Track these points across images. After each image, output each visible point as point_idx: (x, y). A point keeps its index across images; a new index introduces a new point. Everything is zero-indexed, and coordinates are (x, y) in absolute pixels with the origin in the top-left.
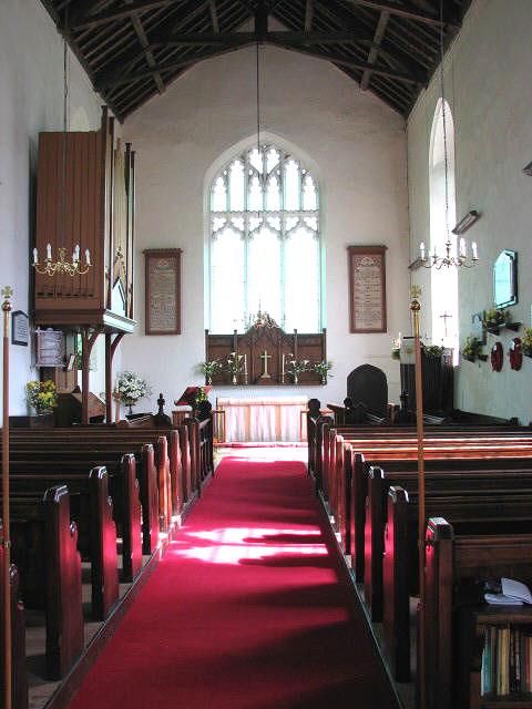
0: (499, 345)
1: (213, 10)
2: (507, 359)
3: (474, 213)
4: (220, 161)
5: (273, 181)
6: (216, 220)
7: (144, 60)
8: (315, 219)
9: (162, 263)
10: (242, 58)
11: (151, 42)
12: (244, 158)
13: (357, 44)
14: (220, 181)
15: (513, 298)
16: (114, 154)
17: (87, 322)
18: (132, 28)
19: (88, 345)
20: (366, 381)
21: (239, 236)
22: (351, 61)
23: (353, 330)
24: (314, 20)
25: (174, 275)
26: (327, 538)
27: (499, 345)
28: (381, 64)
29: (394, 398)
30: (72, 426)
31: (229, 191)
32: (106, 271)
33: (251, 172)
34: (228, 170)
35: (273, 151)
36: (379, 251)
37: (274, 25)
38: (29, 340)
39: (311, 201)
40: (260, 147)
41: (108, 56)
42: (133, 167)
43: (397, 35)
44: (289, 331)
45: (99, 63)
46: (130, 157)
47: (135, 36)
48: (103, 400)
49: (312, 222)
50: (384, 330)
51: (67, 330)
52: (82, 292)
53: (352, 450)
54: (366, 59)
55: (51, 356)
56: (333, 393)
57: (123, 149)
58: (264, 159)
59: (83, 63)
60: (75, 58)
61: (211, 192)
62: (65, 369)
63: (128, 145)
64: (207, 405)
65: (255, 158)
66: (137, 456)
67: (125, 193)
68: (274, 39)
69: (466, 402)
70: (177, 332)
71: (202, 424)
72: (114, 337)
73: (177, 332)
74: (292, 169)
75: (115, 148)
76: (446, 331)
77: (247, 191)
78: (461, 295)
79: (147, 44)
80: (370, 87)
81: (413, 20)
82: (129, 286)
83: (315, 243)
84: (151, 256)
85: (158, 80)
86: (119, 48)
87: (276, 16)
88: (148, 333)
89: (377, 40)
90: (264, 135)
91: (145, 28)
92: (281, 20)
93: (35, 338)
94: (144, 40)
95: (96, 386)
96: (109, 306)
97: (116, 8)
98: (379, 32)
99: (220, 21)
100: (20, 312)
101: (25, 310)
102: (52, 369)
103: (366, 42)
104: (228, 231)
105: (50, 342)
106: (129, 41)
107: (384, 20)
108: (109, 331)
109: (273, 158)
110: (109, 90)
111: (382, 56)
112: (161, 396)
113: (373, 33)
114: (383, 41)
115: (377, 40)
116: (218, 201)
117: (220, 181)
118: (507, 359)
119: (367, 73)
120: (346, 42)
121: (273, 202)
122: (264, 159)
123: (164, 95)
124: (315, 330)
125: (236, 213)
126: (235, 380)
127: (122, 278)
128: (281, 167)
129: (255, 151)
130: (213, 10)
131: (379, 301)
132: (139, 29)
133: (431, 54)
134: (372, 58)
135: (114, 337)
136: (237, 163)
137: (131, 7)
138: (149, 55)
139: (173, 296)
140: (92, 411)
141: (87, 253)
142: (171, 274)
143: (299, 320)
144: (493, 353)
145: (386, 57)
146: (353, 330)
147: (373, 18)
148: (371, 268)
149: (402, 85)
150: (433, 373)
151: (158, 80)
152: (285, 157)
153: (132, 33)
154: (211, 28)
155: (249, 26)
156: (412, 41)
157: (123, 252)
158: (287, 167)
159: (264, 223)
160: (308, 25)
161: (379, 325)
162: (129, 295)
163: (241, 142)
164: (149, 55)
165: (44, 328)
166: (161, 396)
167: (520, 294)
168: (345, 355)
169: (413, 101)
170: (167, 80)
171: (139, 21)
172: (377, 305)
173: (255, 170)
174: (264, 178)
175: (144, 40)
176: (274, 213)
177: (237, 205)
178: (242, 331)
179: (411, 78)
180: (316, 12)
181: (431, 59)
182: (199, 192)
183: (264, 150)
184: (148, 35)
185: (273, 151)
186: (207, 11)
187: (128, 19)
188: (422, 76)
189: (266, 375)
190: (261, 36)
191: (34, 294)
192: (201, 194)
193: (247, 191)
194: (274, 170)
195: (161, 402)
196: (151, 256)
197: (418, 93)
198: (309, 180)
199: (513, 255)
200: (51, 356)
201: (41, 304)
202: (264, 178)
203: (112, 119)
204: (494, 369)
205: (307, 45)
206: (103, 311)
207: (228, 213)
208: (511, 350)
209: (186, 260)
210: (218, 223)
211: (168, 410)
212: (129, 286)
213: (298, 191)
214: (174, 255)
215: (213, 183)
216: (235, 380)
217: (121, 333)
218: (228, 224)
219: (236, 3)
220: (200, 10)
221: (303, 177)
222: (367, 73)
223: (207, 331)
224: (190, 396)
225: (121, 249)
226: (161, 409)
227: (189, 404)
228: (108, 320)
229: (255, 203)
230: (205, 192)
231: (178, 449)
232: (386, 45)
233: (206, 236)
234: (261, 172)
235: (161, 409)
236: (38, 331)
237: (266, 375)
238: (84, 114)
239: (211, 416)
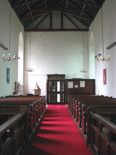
7: (30, 15)
41: (26, 10)
54: (80, 15)
67: (102, 42)
78: (18, 53)
84: (106, 84)
94: (30, 9)
97: (22, 2)
120: (73, 11)
132: (29, 7)
134: (81, 15)
137: (26, 2)
145: (84, 14)
153: (27, 8)
175: (30, 9)
187: (26, 5)
227: (93, 146)
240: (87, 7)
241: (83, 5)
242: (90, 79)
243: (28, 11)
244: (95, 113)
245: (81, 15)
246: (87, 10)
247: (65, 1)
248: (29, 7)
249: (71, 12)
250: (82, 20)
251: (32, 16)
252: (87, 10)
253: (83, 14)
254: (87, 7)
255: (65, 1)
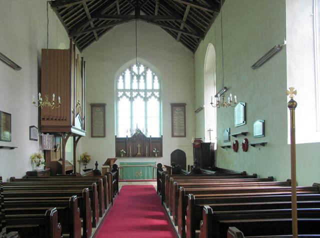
0: (237, 141)
1: (118, 6)
2: (241, 147)
3: (225, 88)
4: (121, 69)
5: (142, 77)
6: (119, 93)
7: (90, 26)
8: (158, 93)
9: (98, 109)
10: (131, 24)
11: (92, 17)
12: (130, 68)
13: (176, 22)
14: (121, 77)
15: (244, 122)
16: (76, 61)
17: (64, 131)
18: (84, 10)
19: (65, 141)
20: (178, 156)
21: (128, 99)
22: (171, 28)
23: (173, 136)
24: (159, 12)
25: (102, 114)
26: (166, 218)
27: (237, 142)
28: (185, 30)
29: (190, 161)
30: (57, 176)
31: (124, 82)
32: (72, 110)
33: (133, 74)
34: (124, 73)
35: (142, 66)
36: (183, 106)
37: (142, 13)
38: (38, 138)
39: (157, 86)
40: (137, 64)
41: (74, 22)
42: (84, 67)
43: (192, 17)
44: (148, 136)
45: (71, 25)
46: (83, 64)
47: (85, 14)
48: (72, 163)
49: (157, 94)
50: (185, 136)
51: (56, 135)
52: (62, 118)
53: (178, 184)
55: (49, 146)
56: (166, 160)
57: (80, 59)
58: (138, 69)
59: (63, 23)
60: (60, 21)
61: (117, 82)
62: (55, 151)
63: (82, 58)
64: (115, 166)
65: (135, 68)
66: (97, 183)
67: (81, 78)
68: (143, 18)
69: (220, 164)
70: (104, 136)
71: (114, 174)
72: (76, 138)
73: (104, 136)
74: (149, 73)
75: (76, 58)
76: (211, 134)
77: (132, 82)
78: (218, 122)
79: (90, 18)
80: (181, 41)
81: (196, 8)
82: (83, 117)
83: (158, 102)
84: (93, 106)
85: (96, 35)
86: (79, 19)
87: (143, 10)
88: (92, 136)
89: (184, 20)
90: (138, 59)
91: (90, 11)
92: (144, 12)
93: (41, 137)
94: (90, 17)
95: (69, 157)
96: (74, 125)
98: (185, 16)
99: (121, 12)
100: (34, 126)
101: (37, 125)
102: (49, 151)
103: (179, 21)
104: (124, 97)
105: (47, 138)
106: (82, 17)
107: (187, 11)
108: (75, 135)
109: (142, 68)
110: (76, 37)
111: (186, 27)
112: (97, 162)
113: (182, 17)
114: (187, 20)
115: (184, 20)
116: (120, 86)
117: (121, 77)
118: (241, 147)
119: (180, 33)
120: (170, 20)
121: (142, 87)
122: (138, 69)
123: (98, 41)
124: (158, 136)
125: (128, 90)
126: (122, 155)
127: (80, 113)
128: (145, 72)
129: (135, 66)
130: (118, 6)
131: (183, 125)
132: (87, 11)
133: (206, 25)
134: (181, 28)
135: (76, 138)
136: (128, 70)
138: (92, 23)
139: (102, 123)
140: (67, 167)
141: (59, 98)
142: (101, 114)
143: (153, 132)
144: (234, 145)
145: (187, 27)
146: (173, 136)
147: (182, 10)
148: (180, 112)
149: (202, 11)
150: (205, 153)
151: (96, 35)
152: (146, 68)
154: (117, 14)
155: (133, 13)
156: (198, 20)
157: (80, 103)
158: (147, 72)
159: (139, 94)
160: (156, 14)
161: (183, 134)
162: (83, 121)
163: (130, 61)
164: (92, 23)
165: (45, 133)
166: (97, 162)
167: (248, 121)
168: (169, 148)
169: (197, 46)
170: (100, 34)
171: (87, 8)
172: (182, 126)
173: (134, 73)
174: (138, 77)
175: (90, 17)
176: (142, 91)
177: (128, 87)
178: (129, 136)
179: (196, 35)
180: (159, 8)
181: (206, 28)
182: (113, 82)
183: (138, 66)
184: (91, 14)
185: (142, 66)
186: (115, 7)
188: (201, 34)
189: (139, 153)
190: (137, 17)
191: (40, 119)
192: (113, 83)
193: (132, 82)
194: (142, 73)
195: (97, 165)
196: (93, 106)
197: (199, 42)
198: (156, 78)
199: (244, 104)
200: (49, 146)
201: (44, 123)
202: (138, 77)
203: (74, 45)
204: (244, 151)
205: (156, 21)
206: (71, 127)
207: (124, 90)
208: (243, 143)
209: (107, 108)
210: (120, 94)
211: (100, 168)
212: (83, 117)
213: (152, 82)
214: (103, 106)
215: (118, 78)
216: (122, 155)
217: (80, 136)
218: (124, 94)
219: (126, 1)
220: (111, 6)
221: (153, 77)
222: (180, 33)
223: (116, 136)
224: (108, 162)
225: (77, 99)
226: (96, 168)
228: (73, 130)
229: (135, 87)
230: (115, 81)
231: (103, 186)
232: (188, 22)
233: (115, 99)
234: (137, 74)
235: (96, 168)
236: (43, 135)
237: (139, 153)
238: (62, 42)
239: (118, 171)
240: (182, 38)
241: (185, 10)
242: (218, 167)
243: (86, 20)
244: (66, 209)
245: (181, 28)
246: (193, 16)
247: (152, 2)
248: (90, 15)
249: (166, 22)
250: (195, 12)
251: (93, 29)
252: (193, 16)
253: (184, 28)
254: (182, 38)
255: (152, 2)
